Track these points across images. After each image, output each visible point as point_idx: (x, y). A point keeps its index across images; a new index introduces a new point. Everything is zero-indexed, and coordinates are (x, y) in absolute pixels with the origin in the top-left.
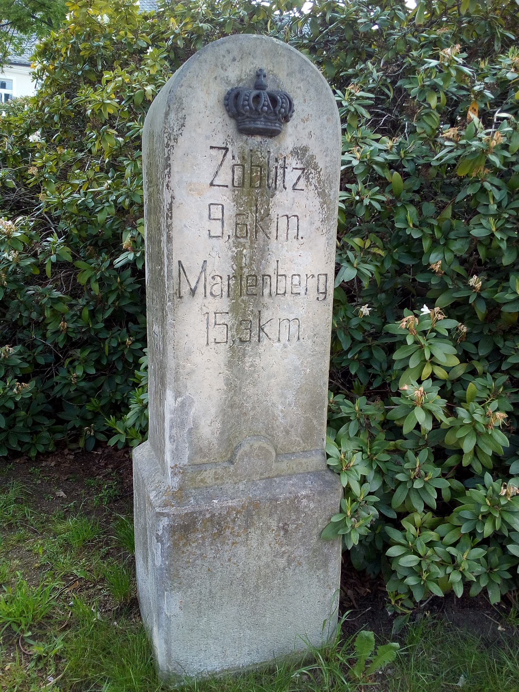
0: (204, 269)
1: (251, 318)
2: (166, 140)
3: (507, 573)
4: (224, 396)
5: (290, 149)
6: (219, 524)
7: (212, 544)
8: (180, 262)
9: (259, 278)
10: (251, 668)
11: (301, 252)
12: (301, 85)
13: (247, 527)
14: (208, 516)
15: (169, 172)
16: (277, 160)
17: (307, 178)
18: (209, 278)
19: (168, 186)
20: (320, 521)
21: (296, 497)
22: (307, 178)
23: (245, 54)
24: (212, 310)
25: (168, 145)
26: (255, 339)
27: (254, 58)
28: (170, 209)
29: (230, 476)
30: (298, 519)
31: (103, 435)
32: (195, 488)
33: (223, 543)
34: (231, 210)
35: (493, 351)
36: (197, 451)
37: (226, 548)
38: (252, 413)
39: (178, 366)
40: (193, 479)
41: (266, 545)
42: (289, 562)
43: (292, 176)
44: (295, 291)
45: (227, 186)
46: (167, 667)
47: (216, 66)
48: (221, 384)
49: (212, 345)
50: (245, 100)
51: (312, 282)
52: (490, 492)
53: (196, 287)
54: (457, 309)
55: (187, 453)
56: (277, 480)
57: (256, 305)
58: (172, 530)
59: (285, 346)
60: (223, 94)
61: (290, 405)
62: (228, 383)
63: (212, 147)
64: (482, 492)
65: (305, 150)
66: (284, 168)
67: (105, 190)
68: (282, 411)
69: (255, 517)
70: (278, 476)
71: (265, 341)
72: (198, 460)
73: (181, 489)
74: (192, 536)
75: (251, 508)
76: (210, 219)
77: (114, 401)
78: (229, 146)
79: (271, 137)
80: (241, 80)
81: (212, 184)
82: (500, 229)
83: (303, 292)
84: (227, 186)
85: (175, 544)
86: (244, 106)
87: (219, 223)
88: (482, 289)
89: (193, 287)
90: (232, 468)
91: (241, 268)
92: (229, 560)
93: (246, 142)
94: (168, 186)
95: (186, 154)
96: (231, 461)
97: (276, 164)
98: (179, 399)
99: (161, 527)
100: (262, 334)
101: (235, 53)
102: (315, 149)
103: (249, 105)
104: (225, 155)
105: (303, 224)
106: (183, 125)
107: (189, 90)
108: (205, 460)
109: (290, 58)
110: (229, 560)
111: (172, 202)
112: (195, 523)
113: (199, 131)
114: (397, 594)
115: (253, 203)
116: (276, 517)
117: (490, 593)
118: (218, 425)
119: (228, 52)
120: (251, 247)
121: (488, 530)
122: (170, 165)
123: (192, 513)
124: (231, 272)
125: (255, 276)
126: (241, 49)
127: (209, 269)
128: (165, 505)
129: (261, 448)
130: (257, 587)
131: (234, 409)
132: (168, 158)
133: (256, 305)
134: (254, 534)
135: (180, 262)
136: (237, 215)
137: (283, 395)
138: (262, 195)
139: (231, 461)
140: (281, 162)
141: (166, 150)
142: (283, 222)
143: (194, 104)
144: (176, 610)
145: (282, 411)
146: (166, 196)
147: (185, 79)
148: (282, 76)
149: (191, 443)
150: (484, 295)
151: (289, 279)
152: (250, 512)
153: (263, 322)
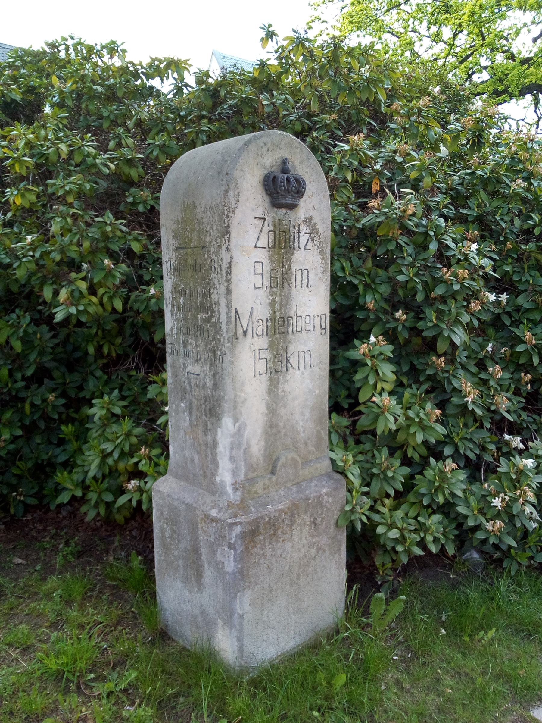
0: (251, 315)
1: (281, 352)
2: (226, 212)
3: (455, 531)
4: (266, 419)
5: (302, 218)
6: (274, 525)
7: (270, 543)
8: (236, 309)
9: (286, 320)
10: (296, 650)
11: (310, 297)
12: (308, 170)
13: (292, 525)
14: (267, 520)
15: (229, 238)
16: (294, 227)
17: (313, 240)
18: (255, 321)
19: (227, 248)
20: (335, 512)
21: (321, 495)
22: (313, 240)
23: (275, 146)
24: (257, 348)
25: (228, 216)
26: (284, 369)
27: (280, 149)
28: (230, 267)
29: (273, 485)
30: (322, 513)
31: (32, 499)
32: (251, 499)
33: (277, 541)
34: (267, 267)
35: (411, 368)
36: (250, 467)
37: (279, 545)
38: (284, 431)
39: (236, 396)
40: (249, 492)
41: (303, 538)
42: (318, 550)
43: (304, 238)
44: (308, 328)
45: (265, 248)
46: (239, 662)
47: (258, 155)
48: (263, 408)
49: (258, 376)
50: (281, 182)
51: (317, 320)
52: (437, 471)
53: (247, 330)
54: (390, 336)
55: (243, 469)
56: (304, 484)
57: (284, 342)
58: (243, 536)
59: (303, 373)
60: (262, 177)
61: (307, 421)
62: (269, 407)
63: (256, 218)
64: (431, 472)
65: (311, 219)
66: (299, 232)
67: (28, 245)
68: (302, 427)
69: (296, 516)
70: (304, 480)
71: (291, 370)
72: (251, 475)
73: (242, 501)
74: (257, 539)
75: (294, 508)
76: (255, 274)
77: (40, 462)
78: (266, 217)
79: (291, 209)
80: (273, 166)
81: (256, 247)
82: (417, 275)
83: (312, 329)
84: (265, 248)
85: (247, 548)
86: (281, 186)
87: (260, 276)
88: (406, 320)
89: (245, 330)
90: (274, 478)
91: (275, 312)
92: (281, 556)
93: (276, 214)
94: (227, 248)
95: (240, 223)
96: (273, 473)
97: (294, 230)
98: (237, 425)
99: (234, 535)
100: (289, 365)
101: (269, 145)
102: (317, 219)
103: (284, 186)
104: (263, 224)
105: (312, 276)
106: (238, 201)
107: (242, 173)
108: (255, 475)
109: (301, 149)
110: (281, 556)
111: (231, 262)
112: (259, 527)
113: (248, 204)
114: (383, 565)
115: (281, 260)
116: (309, 514)
117: (447, 548)
118: (263, 443)
119: (265, 144)
120: (281, 295)
121: (441, 499)
122: (229, 232)
123: (257, 519)
124: (268, 316)
125: (283, 318)
126: (272, 143)
127: (255, 314)
128: (236, 516)
129: (293, 459)
130: (299, 576)
131: (273, 429)
132: (228, 227)
133: (284, 342)
134: (296, 529)
135: (236, 309)
136: (272, 270)
137: (302, 414)
138: (286, 254)
139: (273, 473)
140: (297, 228)
141: (226, 220)
142: (299, 273)
143: (245, 184)
144: (247, 607)
145: (302, 427)
146: (224, 255)
147: (238, 164)
148: (297, 163)
149: (245, 460)
150: (407, 324)
151: (304, 319)
152: (293, 511)
153: (289, 355)
